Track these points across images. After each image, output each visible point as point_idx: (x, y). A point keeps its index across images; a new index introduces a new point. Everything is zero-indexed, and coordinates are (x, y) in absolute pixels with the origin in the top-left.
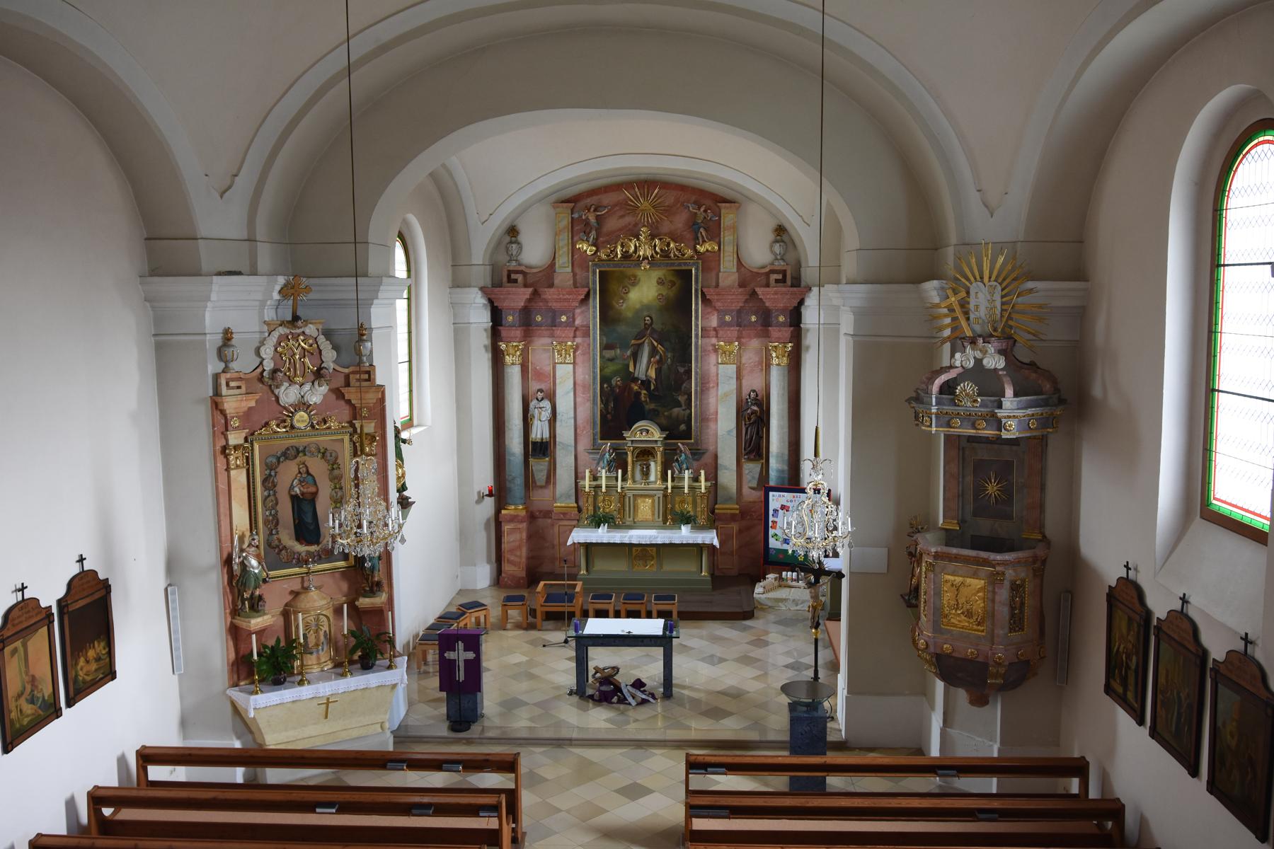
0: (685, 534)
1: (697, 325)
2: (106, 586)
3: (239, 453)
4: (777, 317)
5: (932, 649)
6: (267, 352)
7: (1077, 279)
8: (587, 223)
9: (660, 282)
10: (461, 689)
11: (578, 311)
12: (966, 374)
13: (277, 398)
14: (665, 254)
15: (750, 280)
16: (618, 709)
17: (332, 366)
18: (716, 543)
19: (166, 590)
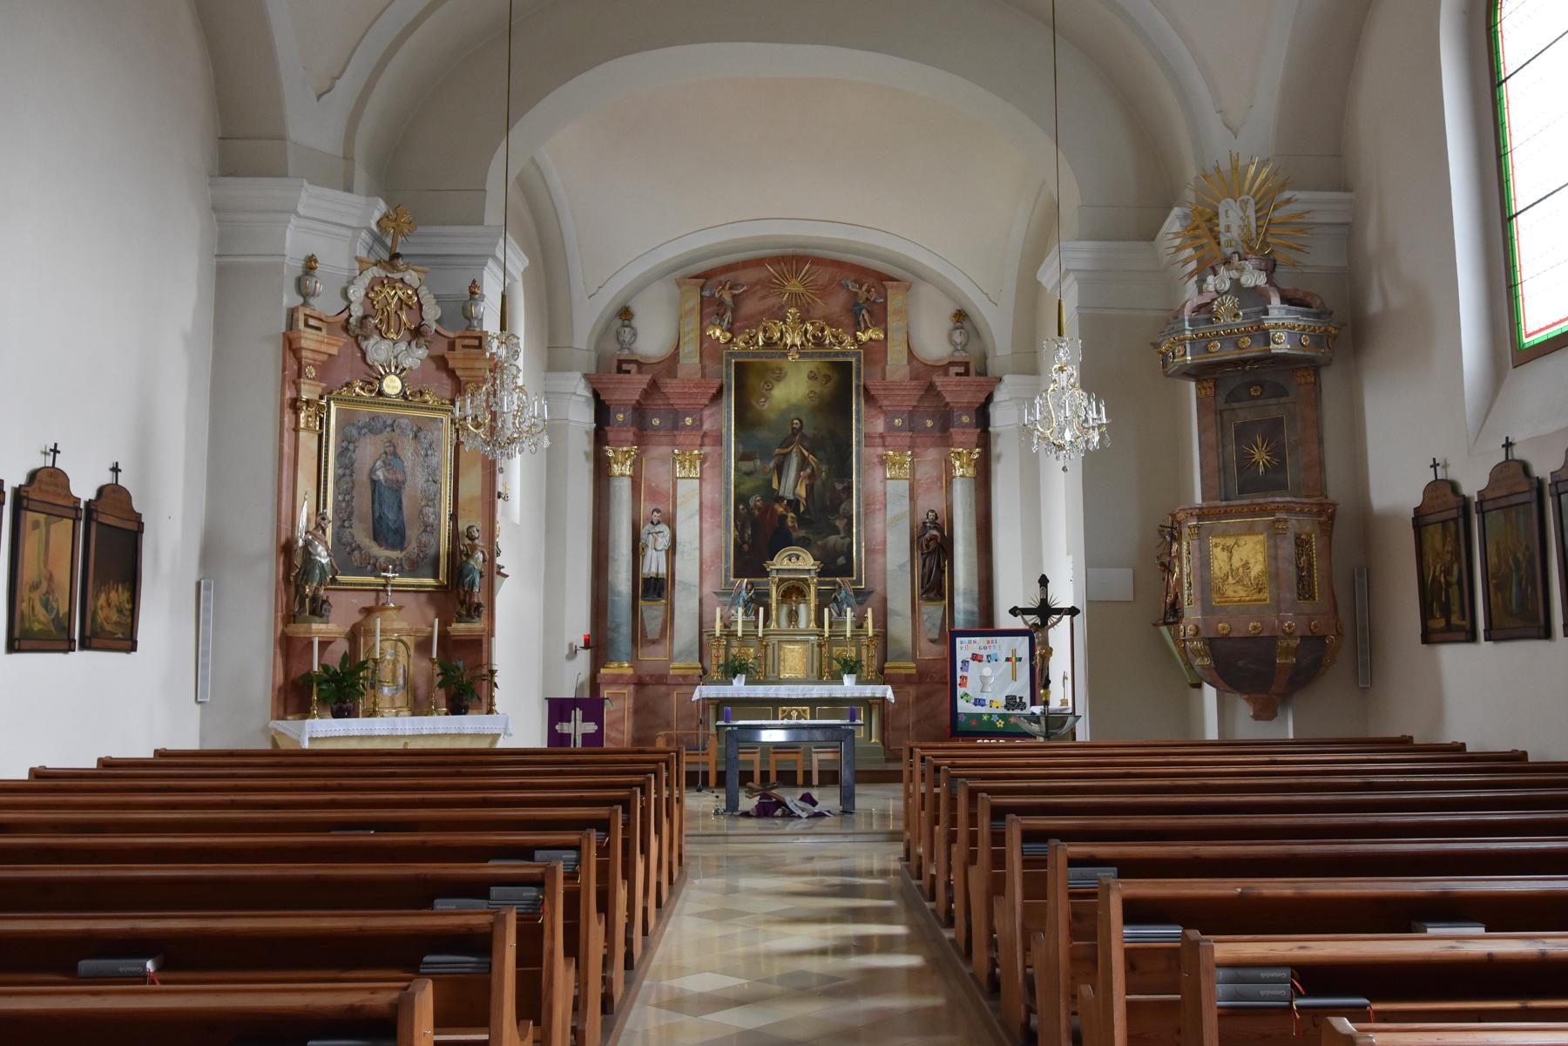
0: (849, 687)
6: (357, 293)
8: (721, 303)
9: (812, 377)
11: (706, 412)
13: (364, 354)
14: (819, 342)
15: (925, 375)
17: (434, 326)
18: (890, 695)
19: (198, 584)
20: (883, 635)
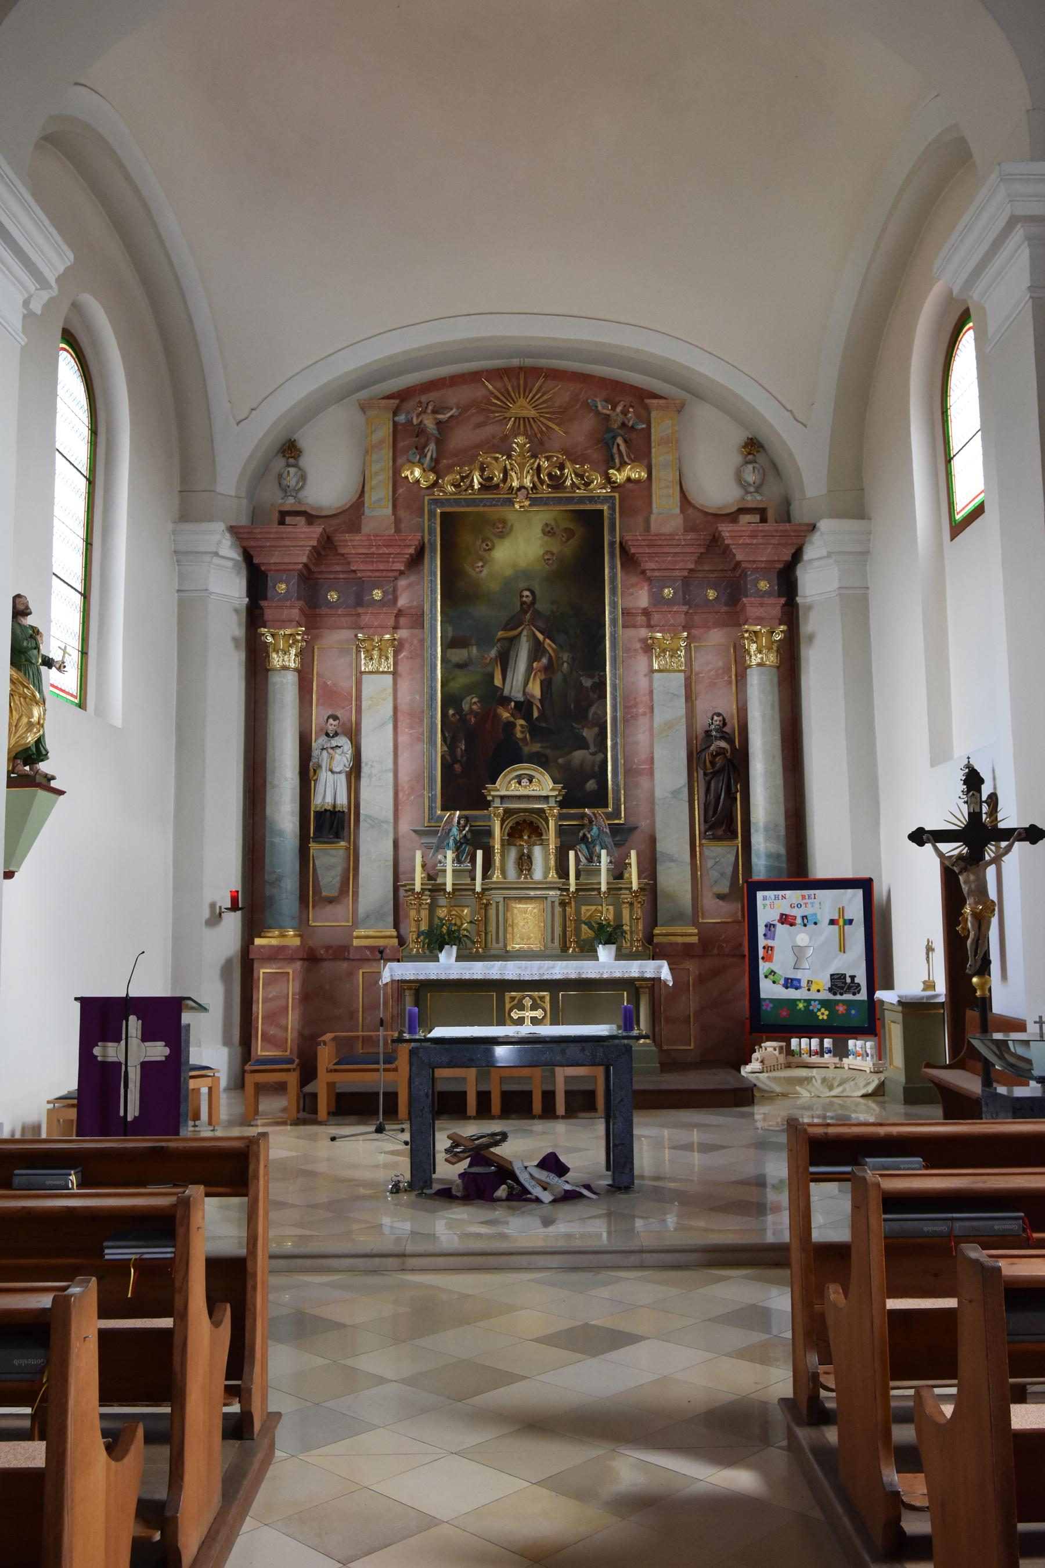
0: (605, 963)
4: (756, 582)
8: (420, 431)
9: (548, 531)
11: (402, 583)
14: (557, 483)
15: (708, 530)
20: (651, 889)
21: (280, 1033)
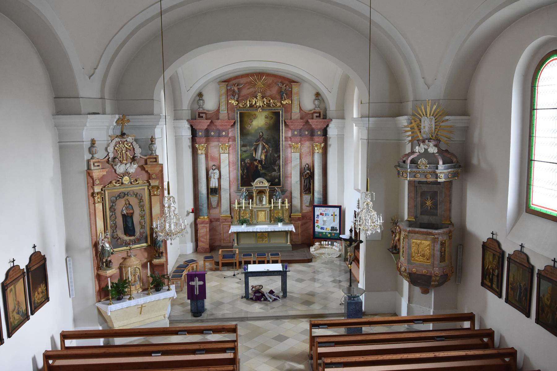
0: (280, 227)
1: (282, 136)
2: (44, 259)
3: (99, 196)
5: (408, 271)
6: (111, 149)
7: (464, 115)
8: (234, 91)
9: (266, 117)
10: (197, 297)
11: (230, 130)
12: (421, 155)
14: (268, 105)
15: (305, 117)
16: (264, 303)
17: (139, 155)
18: (294, 230)
19: (66, 259)
20: (291, 206)
21: (205, 240)
